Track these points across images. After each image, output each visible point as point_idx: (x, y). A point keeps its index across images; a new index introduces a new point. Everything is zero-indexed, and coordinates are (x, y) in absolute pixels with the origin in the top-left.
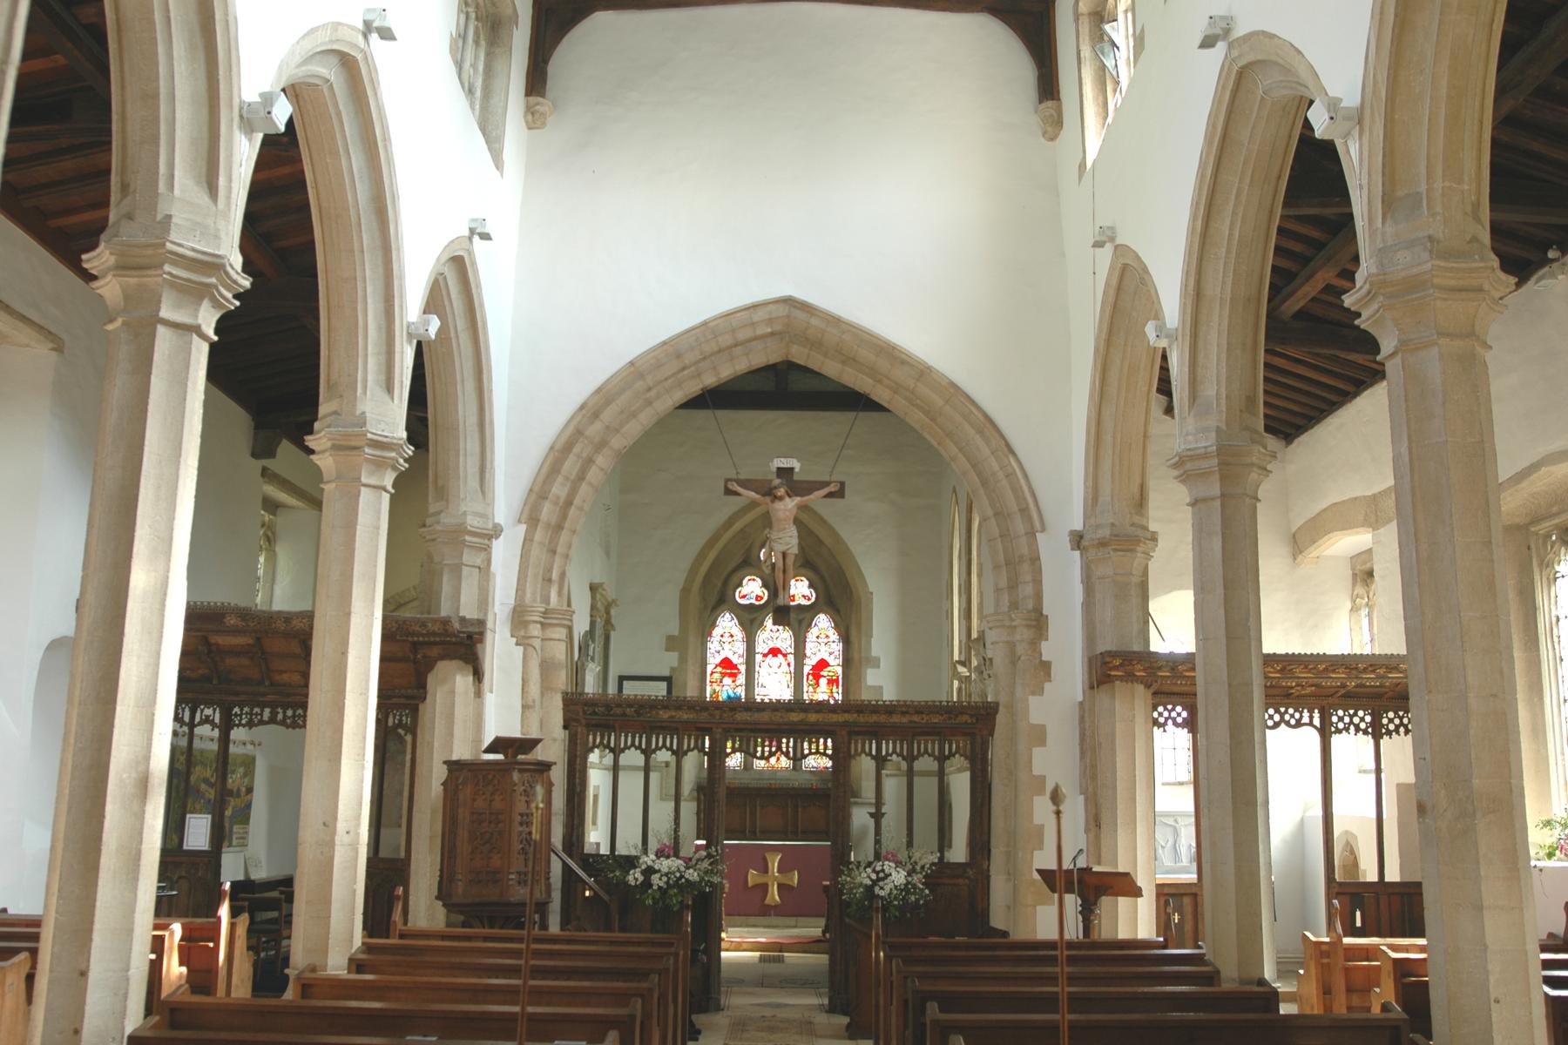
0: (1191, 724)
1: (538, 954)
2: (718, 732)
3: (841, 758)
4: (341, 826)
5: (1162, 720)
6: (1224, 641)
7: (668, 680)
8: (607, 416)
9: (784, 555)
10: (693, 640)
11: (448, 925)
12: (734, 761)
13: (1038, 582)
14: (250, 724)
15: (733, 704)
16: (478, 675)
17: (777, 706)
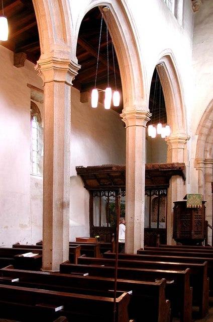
1: (121, 264)
4: (136, 218)
11: (145, 249)
16: (184, 179)
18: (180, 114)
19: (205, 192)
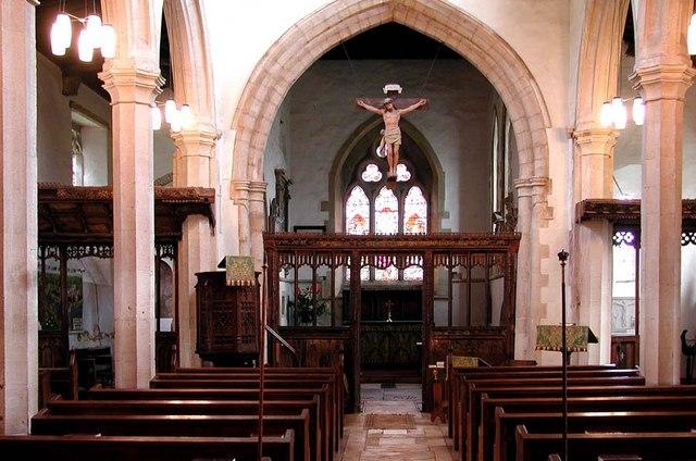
0: (636, 244)
2: (355, 253)
3: (428, 270)
5: (618, 241)
6: (659, 187)
7: (323, 228)
8: (283, 60)
9: (393, 145)
10: (338, 205)
12: (364, 274)
13: (546, 159)
14: (78, 257)
15: (363, 239)
16: (212, 223)
17: (390, 238)
18: (202, 81)
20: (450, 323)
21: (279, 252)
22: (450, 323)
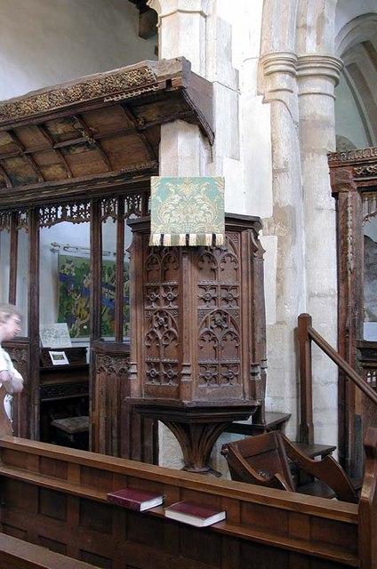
16: (207, 135)
19: (303, 192)
20: (187, 242)
21: (362, 190)
22: (187, 242)
